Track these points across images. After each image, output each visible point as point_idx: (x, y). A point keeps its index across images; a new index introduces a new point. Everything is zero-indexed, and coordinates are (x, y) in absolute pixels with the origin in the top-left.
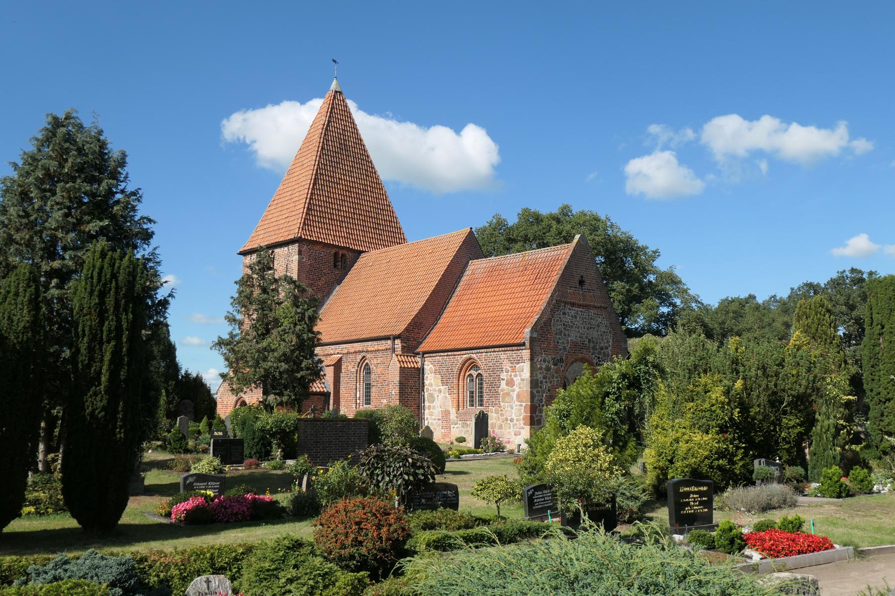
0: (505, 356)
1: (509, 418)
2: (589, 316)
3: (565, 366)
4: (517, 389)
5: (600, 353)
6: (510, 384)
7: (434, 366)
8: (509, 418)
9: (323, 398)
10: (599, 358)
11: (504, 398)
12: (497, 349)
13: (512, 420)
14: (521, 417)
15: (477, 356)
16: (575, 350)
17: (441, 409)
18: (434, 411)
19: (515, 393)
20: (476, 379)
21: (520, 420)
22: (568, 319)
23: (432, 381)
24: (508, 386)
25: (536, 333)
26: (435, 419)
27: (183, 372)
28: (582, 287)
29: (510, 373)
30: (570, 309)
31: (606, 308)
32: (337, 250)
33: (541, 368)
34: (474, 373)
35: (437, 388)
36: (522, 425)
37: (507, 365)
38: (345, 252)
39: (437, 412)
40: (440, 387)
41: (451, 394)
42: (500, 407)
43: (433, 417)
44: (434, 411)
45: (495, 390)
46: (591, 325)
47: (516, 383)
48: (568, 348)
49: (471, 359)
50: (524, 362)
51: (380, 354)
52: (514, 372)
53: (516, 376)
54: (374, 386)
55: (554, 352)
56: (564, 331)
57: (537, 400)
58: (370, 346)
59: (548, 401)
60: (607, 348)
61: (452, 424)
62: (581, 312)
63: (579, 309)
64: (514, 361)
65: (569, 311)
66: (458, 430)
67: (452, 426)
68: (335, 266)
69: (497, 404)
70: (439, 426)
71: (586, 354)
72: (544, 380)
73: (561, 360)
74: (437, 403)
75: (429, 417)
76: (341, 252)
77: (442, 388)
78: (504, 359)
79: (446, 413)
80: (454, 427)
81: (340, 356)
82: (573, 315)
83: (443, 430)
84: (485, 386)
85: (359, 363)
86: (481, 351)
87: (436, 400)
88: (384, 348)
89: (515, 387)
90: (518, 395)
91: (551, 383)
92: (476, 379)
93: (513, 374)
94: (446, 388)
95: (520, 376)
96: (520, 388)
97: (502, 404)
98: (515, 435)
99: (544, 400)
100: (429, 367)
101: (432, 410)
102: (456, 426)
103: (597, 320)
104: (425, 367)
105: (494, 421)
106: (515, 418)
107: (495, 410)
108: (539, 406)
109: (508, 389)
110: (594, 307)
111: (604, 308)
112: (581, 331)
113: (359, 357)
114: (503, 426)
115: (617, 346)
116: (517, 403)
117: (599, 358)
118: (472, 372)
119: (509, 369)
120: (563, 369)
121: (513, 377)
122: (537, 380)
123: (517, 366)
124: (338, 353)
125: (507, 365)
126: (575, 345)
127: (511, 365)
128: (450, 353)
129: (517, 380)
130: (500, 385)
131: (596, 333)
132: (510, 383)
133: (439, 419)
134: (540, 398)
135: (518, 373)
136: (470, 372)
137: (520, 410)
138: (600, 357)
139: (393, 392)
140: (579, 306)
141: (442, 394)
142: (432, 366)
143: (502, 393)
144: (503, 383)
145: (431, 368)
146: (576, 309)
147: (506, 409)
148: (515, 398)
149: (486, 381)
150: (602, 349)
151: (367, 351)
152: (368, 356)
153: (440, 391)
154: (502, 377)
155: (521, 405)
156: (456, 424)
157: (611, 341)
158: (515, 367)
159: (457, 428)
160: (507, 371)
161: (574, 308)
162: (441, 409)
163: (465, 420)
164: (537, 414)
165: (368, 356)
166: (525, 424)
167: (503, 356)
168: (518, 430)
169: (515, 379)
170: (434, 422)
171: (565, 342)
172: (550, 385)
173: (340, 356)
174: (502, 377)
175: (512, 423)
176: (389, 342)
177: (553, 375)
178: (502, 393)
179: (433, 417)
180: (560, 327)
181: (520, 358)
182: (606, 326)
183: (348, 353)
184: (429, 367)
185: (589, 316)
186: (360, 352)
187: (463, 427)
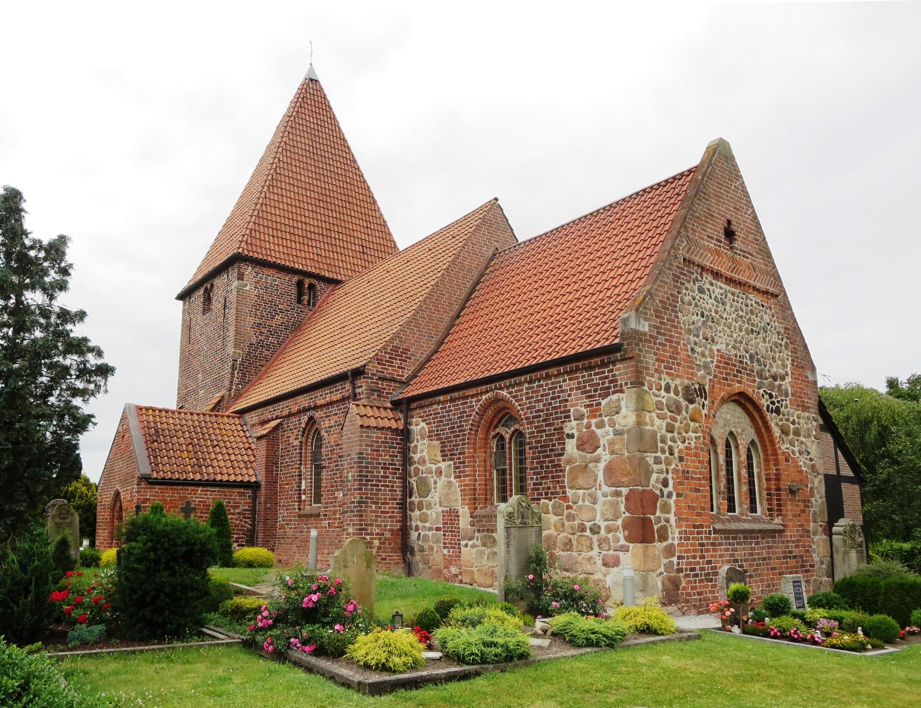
0: (574, 384)
1: (588, 525)
2: (747, 306)
3: (710, 408)
4: (605, 456)
5: (771, 386)
6: (586, 446)
7: (427, 424)
8: (588, 525)
9: (249, 492)
10: (771, 396)
11: (573, 479)
12: (554, 371)
13: (595, 530)
14: (619, 522)
15: (510, 393)
16: (727, 374)
17: (441, 509)
18: (429, 512)
19: (602, 465)
20: (510, 443)
21: (616, 529)
22: (708, 304)
23: (425, 454)
24: (583, 450)
25: (647, 324)
26: (430, 529)
27: (77, 452)
28: (731, 243)
29: (585, 421)
30: (712, 284)
31: (777, 296)
32: (301, 278)
33: (659, 405)
34: (506, 433)
35: (434, 467)
36: (623, 542)
37: (578, 405)
38: (314, 281)
39: (434, 515)
40: (439, 465)
41: (459, 477)
42: (565, 498)
43: (428, 525)
44: (429, 512)
45: (553, 461)
46: (753, 325)
47: (603, 441)
48: (712, 367)
49: (499, 400)
50: (622, 391)
51: (334, 409)
52: (595, 417)
53: (601, 425)
54: (325, 467)
55: (687, 373)
56: (703, 329)
57: (657, 481)
58: (322, 397)
59: (680, 483)
60: (783, 379)
61: (463, 539)
62: (733, 294)
63: (728, 288)
64: (596, 390)
65: (711, 288)
66: (474, 550)
67: (463, 543)
68: (299, 301)
69: (557, 493)
70: (438, 541)
71: (749, 386)
72: (669, 435)
73: (701, 392)
74: (434, 497)
75: (420, 524)
76: (307, 282)
77: (443, 465)
78: (571, 389)
79: (452, 516)
80: (466, 545)
81: (279, 421)
82: (719, 297)
83: (445, 551)
84: (529, 454)
85: (304, 429)
86: (517, 379)
87: (433, 491)
88: (339, 396)
89: (600, 451)
90: (610, 470)
91: (683, 442)
92: (510, 443)
93: (594, 421)
94: (449, 466)
95: (612, 424)
96: (612, 452)
97: (570, 493)
98: (605, 564)
99: (671, 482)
100: (419, 427)
101: (424, 510)
102: (470, 543)
103: (762, 318)
104: (413, 427)
105: (552, 531)
106: (603, 524)
107: (554, 507)
108: (662, 496)
109: (584, 457)
110: (754, 288)
111: (772, 294)
112: (735, 335)
113: (305, 418)
114: (574, 543)
115: (802, 376)
116: (605, 488)
117: (771, 396)
118: (501, 430)
119: (584, 410)
120: (705, 412)
121: (593, 428)
122: (654, 434)
123: (604, 402)
124: (277, 418)
125: (578, 405)
126: (725, 361)
127: (587, 402)
128: (456, 395)
129: (605, 435)
130: (563, 449)
131: (761, 344)
132: (588, 443)
133: (438, 529)
134: (662, 476)
135: (606, 419)
136: (497, 430)
137: (615, 505)
138: (774, 394)
139: (350, 475)
140: (730, 281)
141: (443, 478)
142: (423, 424)
143: (568, 467)
144: (571, 446)
145: (423, 428)
146: (723, 286)
147: (580, 503)
148: (601, 477)
149: (529, 443)
150: (775, 378)
151: (316, 408)
152: (317, 415)
153: (439, 472)
154: (567, 431)
155: (618, 494)
156: (470, 539)
157: (789, 363)
158: (599, 404)
159: (473, 546)
160: (580, 417)
161: (719, 284)
162: (441, 509)
163: (488, 531)
164: (658, 513)
165: (317, 415)
166: (629, 539)
167: (567, 384)
168: (611, 552)
169: (599, 432)
170: (430, 534)
171: (707, 353)
172: (681, 446)
173: (279, 421)
174: (567, 431)
175: (595, 538)
176: (348, 385)
177: (688, 425)
178: (568, 467)
179: (428, 525)
180: (695, 318)
181: (611, 382)
182: (778, 333)
183: (291, 415)
184: (419, 427)
185: (747, 306)
186: (306, 410)
187: (484, 545)
